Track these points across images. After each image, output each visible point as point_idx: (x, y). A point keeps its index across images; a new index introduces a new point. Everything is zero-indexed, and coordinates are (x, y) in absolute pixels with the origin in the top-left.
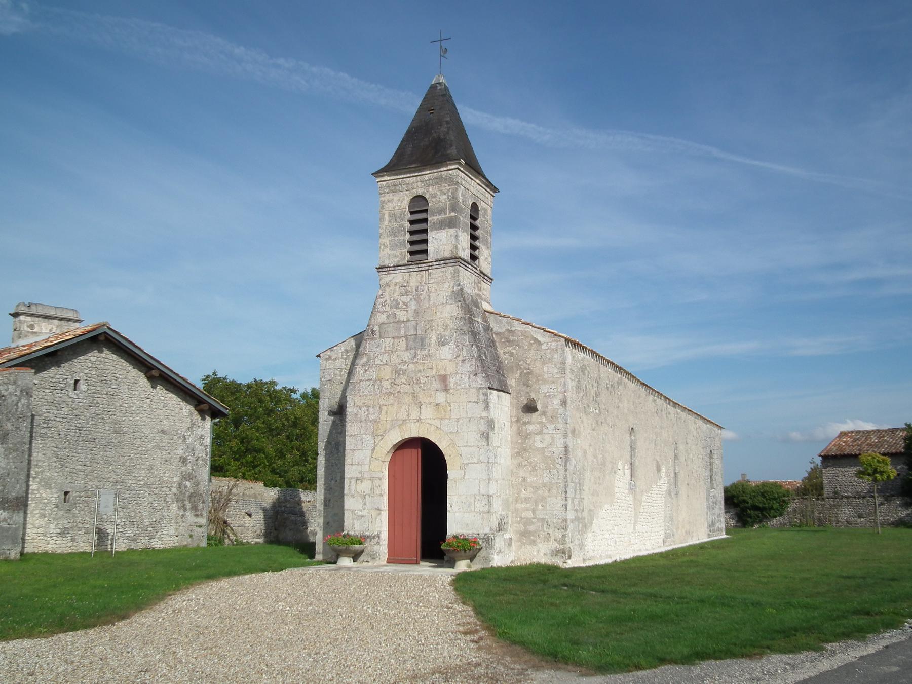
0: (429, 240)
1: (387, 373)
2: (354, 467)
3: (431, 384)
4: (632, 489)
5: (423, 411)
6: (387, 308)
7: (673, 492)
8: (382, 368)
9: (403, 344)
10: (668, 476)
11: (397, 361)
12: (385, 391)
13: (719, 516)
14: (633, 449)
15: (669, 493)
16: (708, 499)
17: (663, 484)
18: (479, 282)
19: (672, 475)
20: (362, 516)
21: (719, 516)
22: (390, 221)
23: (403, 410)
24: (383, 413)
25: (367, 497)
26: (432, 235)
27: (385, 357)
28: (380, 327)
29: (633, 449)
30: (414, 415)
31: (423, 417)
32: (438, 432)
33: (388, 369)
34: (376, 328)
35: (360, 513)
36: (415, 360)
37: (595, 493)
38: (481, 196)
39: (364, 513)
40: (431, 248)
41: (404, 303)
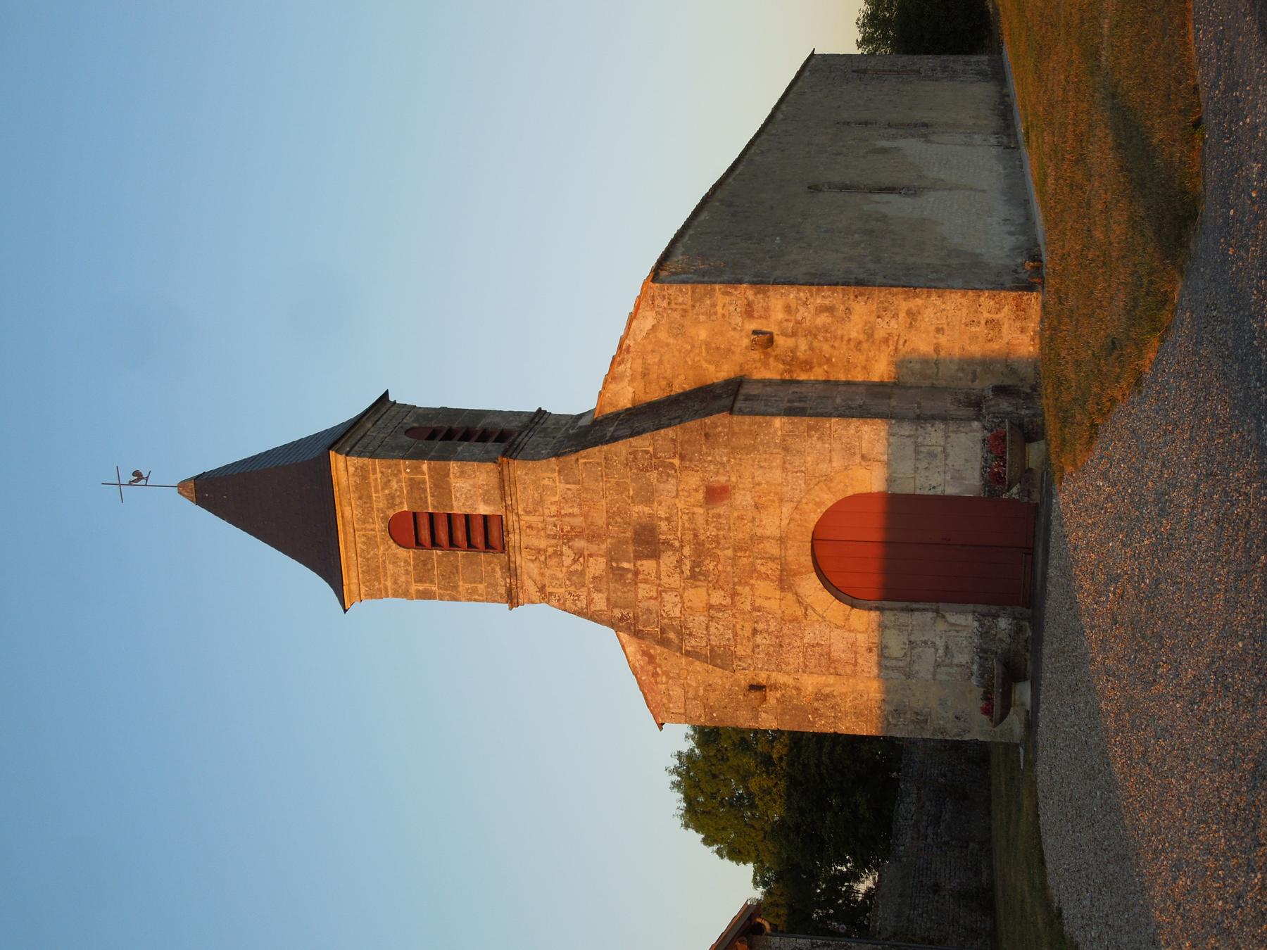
0: (468, 511)
1: (697, 596)
2: (860, 661)
3: (719, 516)
4: (912, 191)
5: (768, 533)
6: (583, 593)
7: (923, 129)
8: (687, 604)
9: (648, 565)
10: (894, 137)
11: (677, 577)
12: (728, 600)
13: (967, 63)
14: (845, 188)
15: (926, 138)
16: (937, 80)
17: (911, 146)
18: (544, 430)
19: (893, 131)
20: (947, 647)
21: (967, 63)
22: (432, 582)
23: (763, 569)
24: (766, 604)
25: (912, 639)
26: (459, 507)
27: (669, 598)
28: (615, 606)
29: (845, 188)
30: (773, 548)
31: (777, 534)
32: (803, 506)
33: (690, 594)
34: (617, 613)
35: (941, 652)
36: (677, 544)
37: (974, 612)
38: (395, 422)
39: (940, 643)
40: (483, 509)
41: (575, 561)
